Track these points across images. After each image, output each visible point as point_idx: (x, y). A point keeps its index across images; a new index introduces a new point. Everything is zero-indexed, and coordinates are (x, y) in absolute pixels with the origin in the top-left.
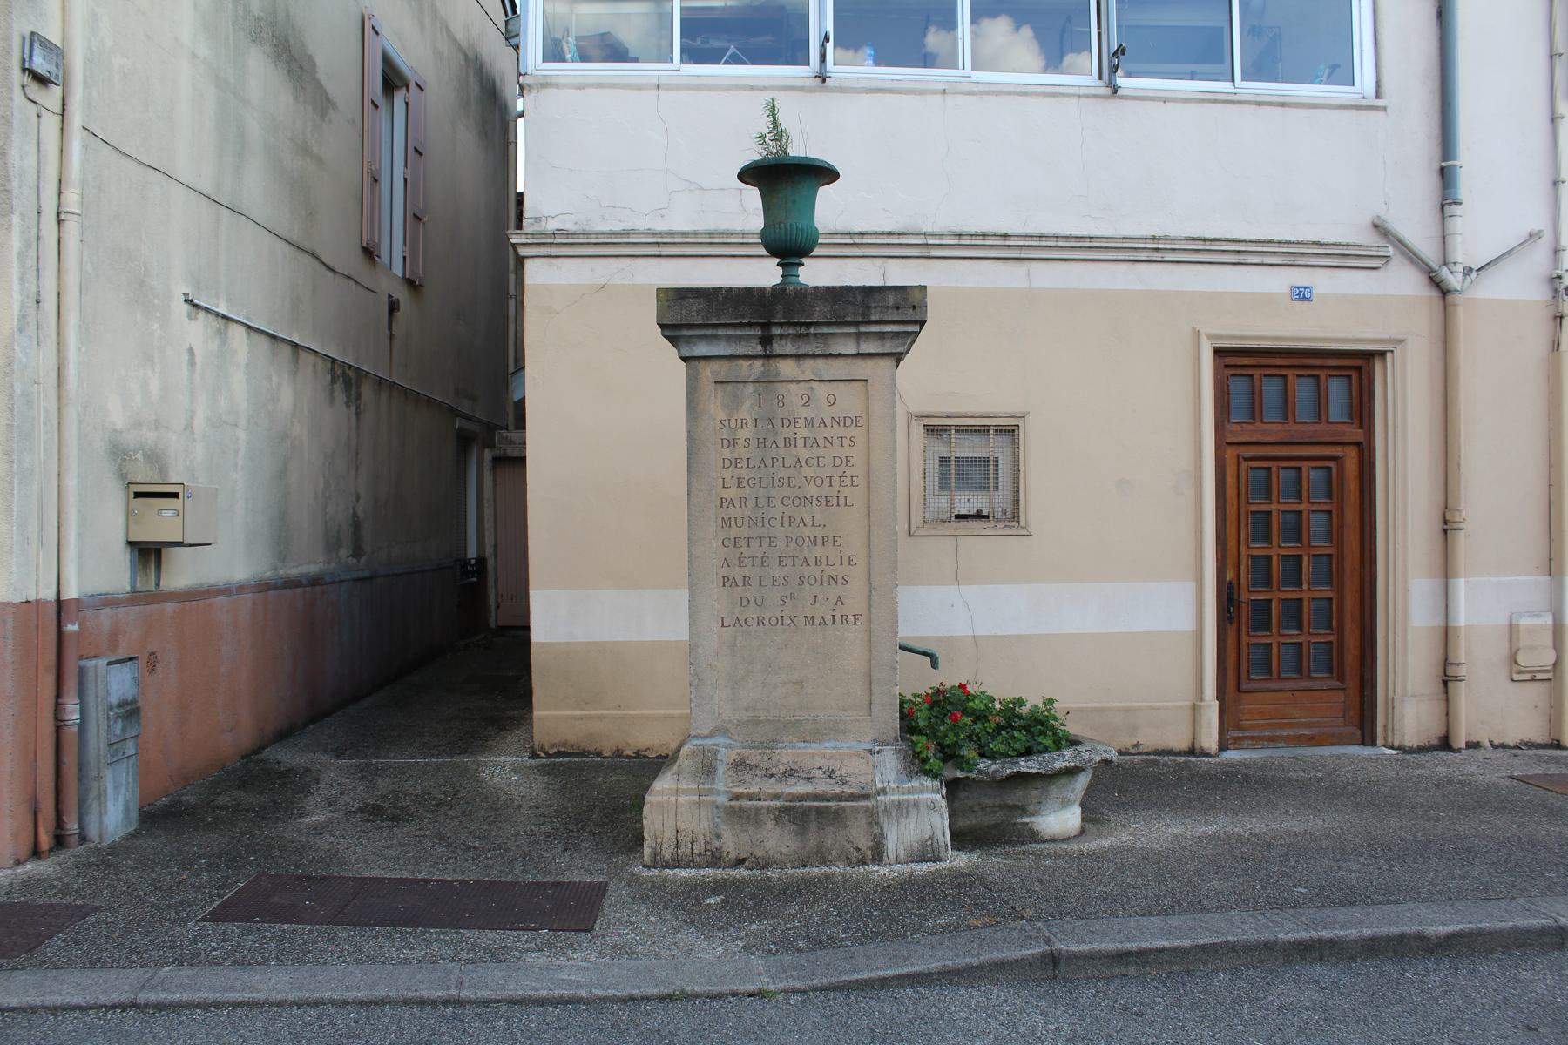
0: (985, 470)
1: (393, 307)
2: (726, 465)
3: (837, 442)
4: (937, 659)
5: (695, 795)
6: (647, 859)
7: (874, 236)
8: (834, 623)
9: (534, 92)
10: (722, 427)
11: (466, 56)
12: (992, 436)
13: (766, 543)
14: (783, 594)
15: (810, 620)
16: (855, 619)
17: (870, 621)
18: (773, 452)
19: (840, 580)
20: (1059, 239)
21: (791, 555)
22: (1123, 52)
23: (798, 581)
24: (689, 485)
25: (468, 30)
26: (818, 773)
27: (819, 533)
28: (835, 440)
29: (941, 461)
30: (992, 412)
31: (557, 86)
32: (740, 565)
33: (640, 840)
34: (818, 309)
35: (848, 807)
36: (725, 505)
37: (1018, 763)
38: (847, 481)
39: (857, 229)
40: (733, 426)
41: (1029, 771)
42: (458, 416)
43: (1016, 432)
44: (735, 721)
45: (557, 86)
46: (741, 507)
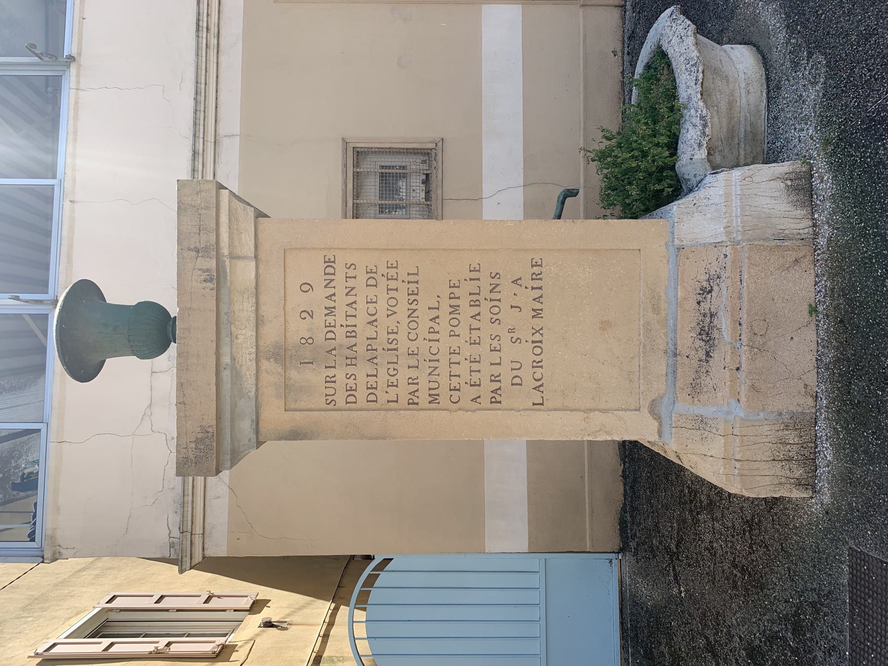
1: (269, 624)
3: (351, 283)
4: (568, 190)
8: (540, 288)
12: (362, 170)
15: (537, 313)
18: (361, 349)
19: (495, 281)
20: (198, 109)
26: (705, 306)
28: (348, 285)
29: (382, 212)
38: (392, 272)
40: (332, 392)
43: (358, 149)
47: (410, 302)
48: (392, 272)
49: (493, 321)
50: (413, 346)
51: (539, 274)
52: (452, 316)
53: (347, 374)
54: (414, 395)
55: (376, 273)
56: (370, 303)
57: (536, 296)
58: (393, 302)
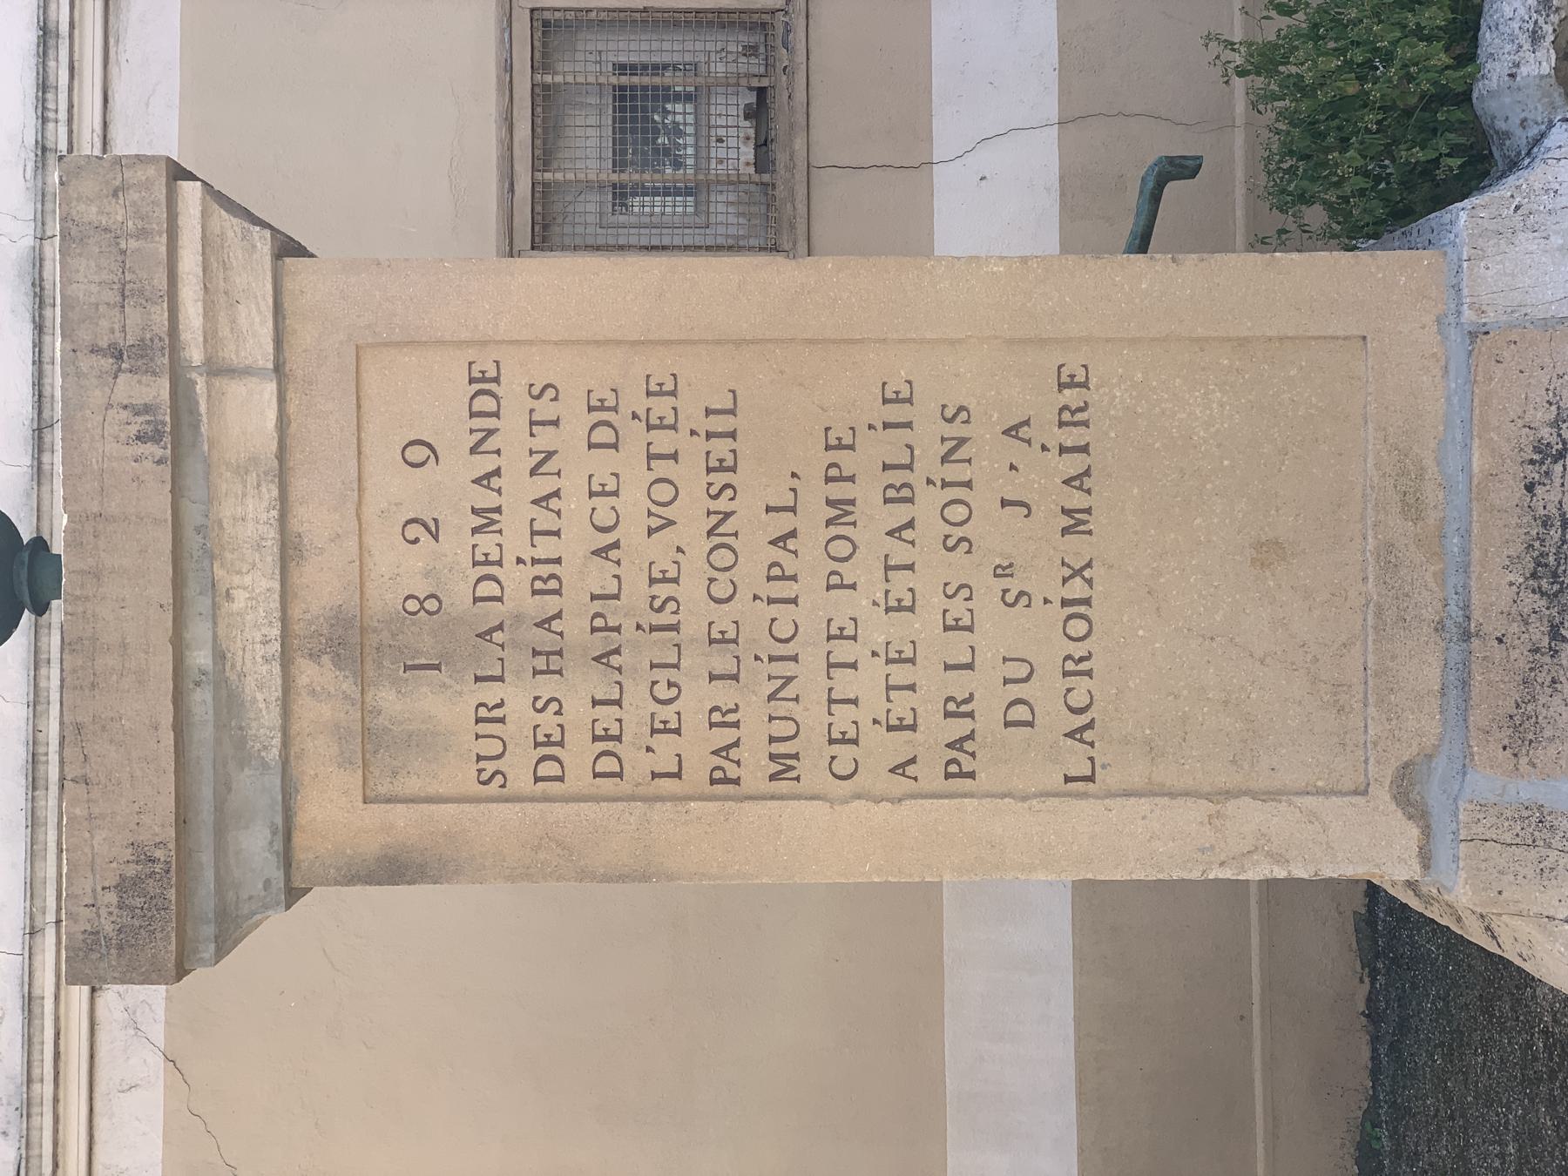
0: (634, 98)
3: (546, 439)
4: (1171, 160)
8: (1084, 449)
14: (997, 599)
18: (575, 627)
38: (662, 407)
40: (496, 748)
43: (547, 15)
47: (714, 491)
48: (662, 407)
49: (951, 543)
50: (724, 619)
53: (536, 698)
54: (727, 758)
55: (615, 409)
56: (598, 494)
57: (1073, 472)
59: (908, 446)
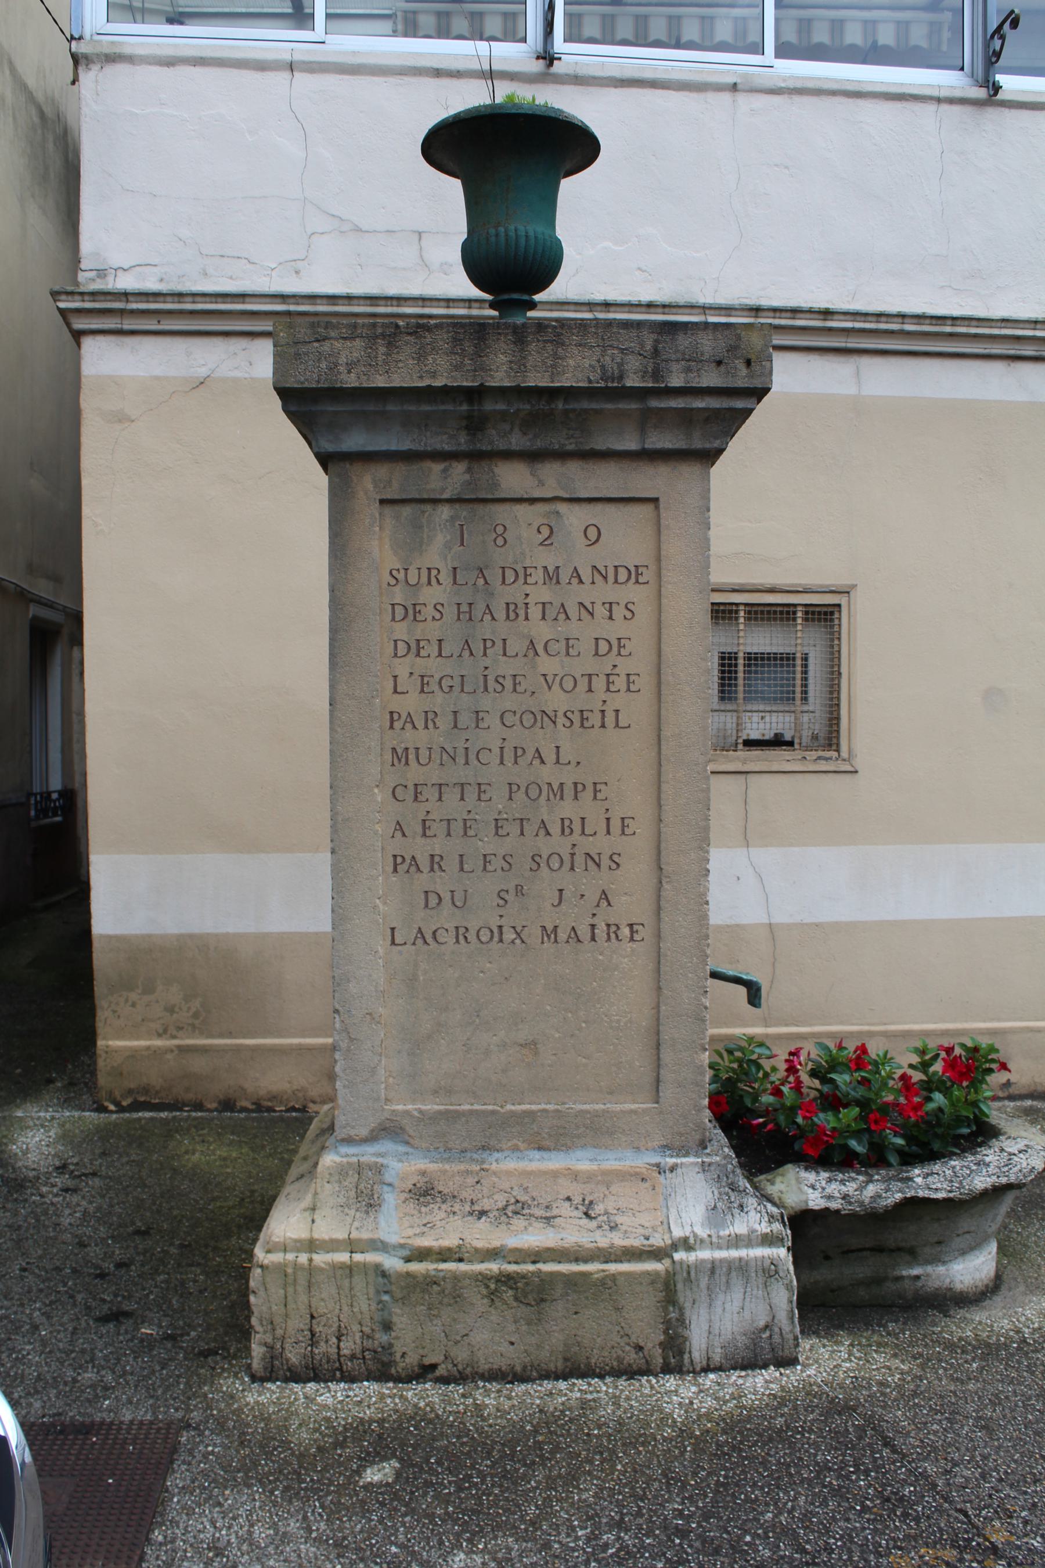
2: (398, 617)
3: (601, 611)
4: (759, 989)
5: (344, 1251)
6: (256, 1364)
7: (627, 309)
8: (593, 939)
9: (95, 68)
10: (393, 582)
11: (42, 115)
13: (471, 794)
15: (550, 934)
16: (632, 932)
17: (658, 936)
19: (605, 862)
21: (517, 816)
22: (1015, 24)
23: (529, 864)
24: (332, 687)
25: (45, 77)
26: (565, 1209)
27: (568, 776)
30: (800, 585)
31: (129, 59)
32: (424, 835)
33: (245, 1333)
34: (571, 362)
35: (621, 1274)
36: (398, 725)
37: (910, 1179)
38: (620, 683)
39: (599, 297)
40: (413, 581)
41: (934, 1196)
42: (32, 601)
43: (836, 615)
44: (416, 1114)
45: (129, 59)
46: (426, 727)
47: (569, 714)
48: (620, 683)
49: (537, 859)
50: (492, 721)
51: (617, 937)
52: (545, 788)
54: (406, 722)
55: (619, 654)
56: (567, 644)
57: (579, 933)
58: (568, 684)
59: (595, 833)
